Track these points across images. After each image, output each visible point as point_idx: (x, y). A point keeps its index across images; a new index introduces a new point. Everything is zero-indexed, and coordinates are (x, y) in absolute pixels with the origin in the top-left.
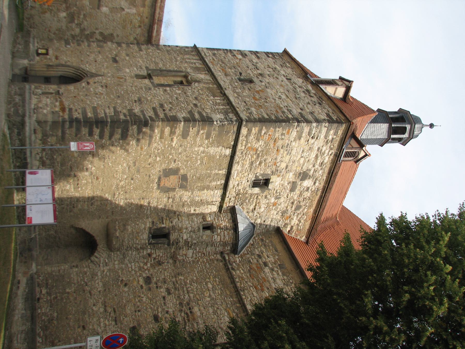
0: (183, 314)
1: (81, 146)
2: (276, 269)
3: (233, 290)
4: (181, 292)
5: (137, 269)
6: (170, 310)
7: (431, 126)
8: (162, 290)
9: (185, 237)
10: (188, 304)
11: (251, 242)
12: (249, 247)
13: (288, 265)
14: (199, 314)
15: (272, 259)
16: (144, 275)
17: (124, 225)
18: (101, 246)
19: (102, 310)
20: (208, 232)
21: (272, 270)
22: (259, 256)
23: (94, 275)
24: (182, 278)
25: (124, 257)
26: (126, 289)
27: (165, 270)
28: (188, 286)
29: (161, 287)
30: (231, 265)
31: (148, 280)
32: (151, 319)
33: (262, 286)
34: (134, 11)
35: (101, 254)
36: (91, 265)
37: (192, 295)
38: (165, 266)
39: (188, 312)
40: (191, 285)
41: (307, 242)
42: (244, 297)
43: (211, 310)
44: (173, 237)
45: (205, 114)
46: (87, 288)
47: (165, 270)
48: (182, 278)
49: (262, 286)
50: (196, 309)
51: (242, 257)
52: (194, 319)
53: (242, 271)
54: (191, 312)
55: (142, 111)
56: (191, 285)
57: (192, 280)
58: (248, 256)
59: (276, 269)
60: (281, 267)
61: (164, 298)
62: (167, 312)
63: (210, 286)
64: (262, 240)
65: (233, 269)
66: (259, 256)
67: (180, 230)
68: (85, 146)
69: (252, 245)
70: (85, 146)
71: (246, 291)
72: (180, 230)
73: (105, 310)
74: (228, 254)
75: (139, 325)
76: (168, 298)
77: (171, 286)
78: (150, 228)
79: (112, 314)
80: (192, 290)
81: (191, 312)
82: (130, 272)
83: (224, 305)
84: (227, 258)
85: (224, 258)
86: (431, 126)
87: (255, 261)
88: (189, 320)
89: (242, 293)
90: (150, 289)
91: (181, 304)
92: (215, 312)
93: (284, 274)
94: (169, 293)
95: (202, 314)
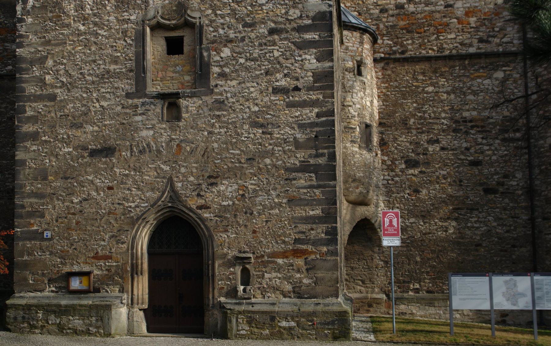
0: (472, 132)
3: (440, 63)
4: (436, 127)
5: (392, 174)
6: (465, 145)
8: (430, 149)
10: (456, 122)
14: (475, 113)
16: (403, 166)
24: (412, 120)
28: (426, 115)
31: (411, 164)
37: (443, 115)
39: (470, 124)
40: (425, 112)
42: (454, 52)
43: (471, 97)
48: (412, 120)
50: (466, 114)
52: (483, 120)
53: (410, 42)
54: (471, 121)
56: (425, 112)
58: (381, 26)
62: (467, 149)
63: (430, 89)
65: (403, 53)
68: (391, 224)
70: (391, 224)
71: (445, 46)
75: (481, 184)
77: (425, 137)
79: (463, 212)
80: (434, 112)
81: (471, 121)
82: (396, 182)
84: (383, 55)
87: (391, 19)
88: (482, 127)
89: (447, 53)
92: (475, 93)
94: (437, 141)
95: (474, 109)
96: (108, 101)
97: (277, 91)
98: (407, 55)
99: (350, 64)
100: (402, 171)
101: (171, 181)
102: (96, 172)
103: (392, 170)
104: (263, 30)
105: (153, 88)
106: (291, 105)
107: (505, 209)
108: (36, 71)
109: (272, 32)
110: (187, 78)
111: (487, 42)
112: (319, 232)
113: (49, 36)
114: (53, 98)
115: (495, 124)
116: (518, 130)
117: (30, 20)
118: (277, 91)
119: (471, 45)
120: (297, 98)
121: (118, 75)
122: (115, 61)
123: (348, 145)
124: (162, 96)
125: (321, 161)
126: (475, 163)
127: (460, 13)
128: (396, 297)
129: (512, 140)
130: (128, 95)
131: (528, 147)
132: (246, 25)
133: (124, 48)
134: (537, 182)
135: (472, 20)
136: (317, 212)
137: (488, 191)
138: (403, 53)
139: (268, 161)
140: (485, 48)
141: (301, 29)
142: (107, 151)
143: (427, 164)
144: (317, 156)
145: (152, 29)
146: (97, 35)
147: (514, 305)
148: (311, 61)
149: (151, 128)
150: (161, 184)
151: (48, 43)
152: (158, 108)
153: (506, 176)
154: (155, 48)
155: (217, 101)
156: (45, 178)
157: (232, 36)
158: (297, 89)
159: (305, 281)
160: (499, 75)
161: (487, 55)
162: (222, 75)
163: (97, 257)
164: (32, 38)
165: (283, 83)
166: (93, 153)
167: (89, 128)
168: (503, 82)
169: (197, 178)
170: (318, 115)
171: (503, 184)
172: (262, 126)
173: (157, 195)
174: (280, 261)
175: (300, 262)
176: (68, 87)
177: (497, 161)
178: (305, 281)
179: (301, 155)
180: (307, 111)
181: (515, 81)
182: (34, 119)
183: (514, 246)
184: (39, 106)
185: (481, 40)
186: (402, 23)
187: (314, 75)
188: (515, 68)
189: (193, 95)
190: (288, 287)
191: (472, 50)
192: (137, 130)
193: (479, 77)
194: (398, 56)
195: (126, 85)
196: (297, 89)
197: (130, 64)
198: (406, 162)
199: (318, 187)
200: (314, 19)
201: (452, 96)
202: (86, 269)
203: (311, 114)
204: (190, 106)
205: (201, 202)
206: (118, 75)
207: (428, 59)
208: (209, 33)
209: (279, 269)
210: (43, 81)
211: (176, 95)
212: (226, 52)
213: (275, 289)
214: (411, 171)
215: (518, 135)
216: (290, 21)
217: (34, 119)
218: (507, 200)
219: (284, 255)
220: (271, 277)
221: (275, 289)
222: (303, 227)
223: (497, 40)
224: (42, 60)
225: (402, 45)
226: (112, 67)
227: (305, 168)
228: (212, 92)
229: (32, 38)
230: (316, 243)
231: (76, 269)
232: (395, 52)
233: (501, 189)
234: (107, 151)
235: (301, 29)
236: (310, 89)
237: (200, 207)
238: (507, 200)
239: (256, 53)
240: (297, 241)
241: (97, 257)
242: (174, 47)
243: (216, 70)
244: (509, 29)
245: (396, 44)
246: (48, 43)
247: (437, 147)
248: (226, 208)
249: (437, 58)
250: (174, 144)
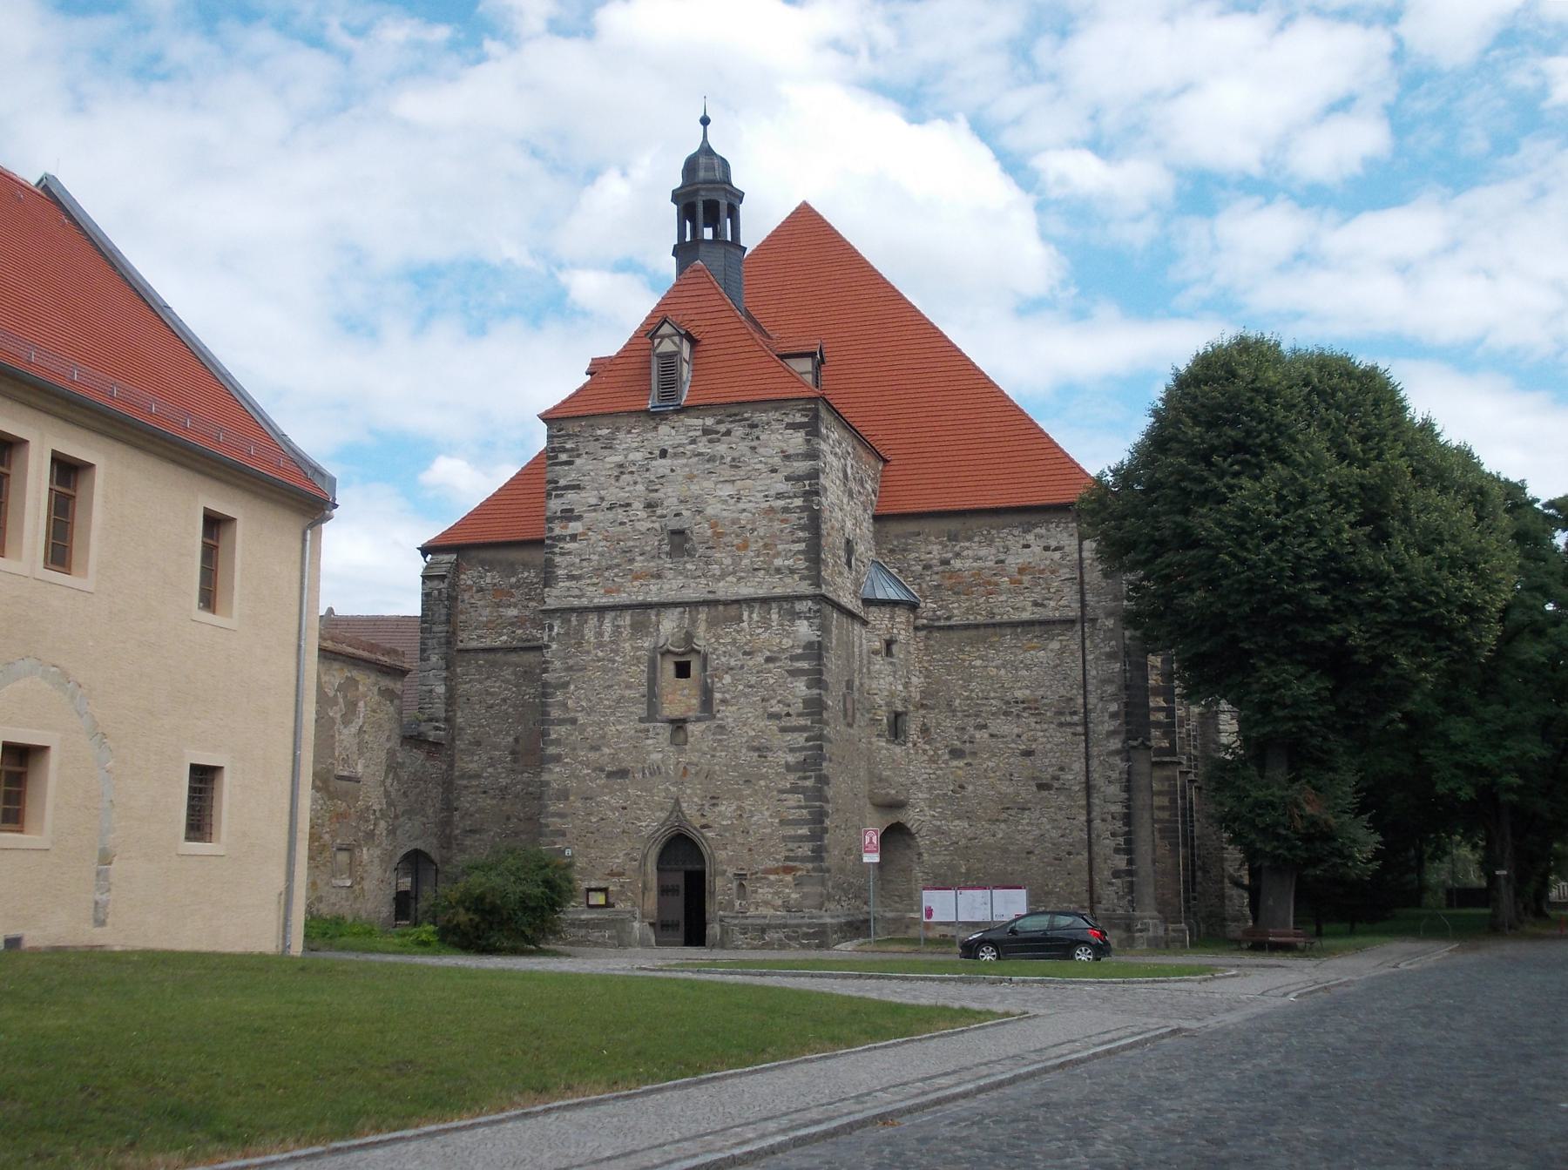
1: (871, 848)
2: (957, 549)
3: (990, 631)
6: (1016, 731)
7: (705, 121)
9: (900, 688)
10: (1008, 703)
11: (894, 571)
12: (906, 577)
13: (953, 525)
14: (1028, 692)
15: (936, 549)
16: (947, 757)
17: (880, 780)
18: (901, 817)
19: (1003, 826)
20: (895, 648)
21: (958, 555)
22: (927, 567)
23: (938, 831)
25: (870, 772)
26: (970, 788)
27: (939, 724)
29: (972, 737)
30: (939, 619)
31: (956, 753)
32: (1027, 761)
33: (989, 583)
34: (361, 704)
35: (911, 818)
36: (923, 833)
38: (931, 723)
41: (886, 461)
44: (900, 709)
45: (800, 651)
46: (963, 842)
47: (939, 724)
49: (989, 583)
50: (1019, 694)
51: (926, 597)
52: (1036, 701)
55: (792, 750)
57: (964, 687)
59: (957, 549)
60: (953, 537)
61: (992, 736)
62: (1019, 736)
63: (978, 663)
64: (892, 551)
65: (948, 618)
66: (926, 567)
67: (892, 694)
69: (900, 571)
72: (892, 694)
73: (1005, 821)
74: (916, 618)
76: (993, 730)
77: (972, 721)
78: (888, 741)
79: (1012, 812)
83: (1018, 651)
85: (924, 627)
86: (705, 121)
87: (935, 577)
90: (974, 754)
91: (1006, 714)
93: (970, 539)
94: (985, 727)
95: (1027, 687)
96: (623, 726)
97: (772, 716)
98: (952, 622)
99: (877, 645)
100: (946, 762)
101: (677, 802)
102: (612, 793)
103: (935, 762)
104: (760, 659)
105: (671, 709)
106: (783, 730)
107: (1060, 809)
108: (559, 696)
109: (768, 660)
110: (694, 701)
111: (1042, 605)
112: (806, 849)
113: (571, 662)
114: (574, 721)
115: (1050, 705)
116: (1075, 713)
117: (554, 646)
118: (772, 716)
119: (1024, 609)
120: (785, 722)
121: (634, 701)
122: (629, 686)
123: (874, 739)
124: (672, 721)
125: (809, 783)
126: (1028, 753)
127: (1013, 569)
128: (663, 928)
129: (1070, 724)
130: (641, 720)
131: (1086, 734)
132: (745, 653)
133: (639, 673)
134: (1096, 776)
135: (1026, 579)
136: (804, 831)
137: (1042, 786)
138: (948, 618)
139: (762, 783)
140: (1040, 614)
141: (793, 658)
142: (623, 773)
143: (974, 754)
144: (805, 778)
145: (663, 655)
146: (614, 662)
147: (678, 925)
148: (801, 687)
149: (657, 747)
150: (670, 804)
151: (570, 669)
152: (665, 731)
153: (1062, 769)
154: (669, 668)
155: (719, 726)
156: (567, 799)
157: (733, 663)
158: (788, 715)
159: (794, 896)
160: (1055, 645)
161: (1041, 623)
162: (724, 701)
163: (612, 874)
164: (558, 664)
165: (776, 709)
166: (610, 775)
167: (606, 750)
168: (1062, 650)
169: (702, 798)
170: (807, 740)
171: (1057, 778)
172: (758, 749)
173: (664, 815)
174: (772, 877)
175: (789, 878)
176: (589, 711)
177: (1051, 750)
178: (794, 896)
179: (791, 777)
180: (796, 735)
181: (1072, 654)
182: (557, 742)
183: (1069, 853)
184: (563, 729)
185: (1036, 604)
186: (947, 583)
187: (805, 702)
188: (1072, 638)
189: (698, 720)
190: (780, 902)
191: (1026, 616)
192: (648, 753)
193: (1033, 648)
194: (942, 623)
195: (641, 710)
196: (788, 715)
197: (643, 690)
198: (951, 752)
199: (805, 807)
200: (805, 648)
201: (1003, 672)
202: (603, 885)
203: (800, 739)
204: (694, 729)
205: (704, 821)
206: (634, 701)
207: (977, 626)
208: (714, 662)
209: (771, 885)
210: (565, 705)
211: (684, 721)
212: (727, 679)
213: (766, 903)
214: (955, 763)
215: (1076, 718)
216: (784, 651)
217: (557, 742)
218: (1062, 798)
219: (775, 871)
220: (764, 892)
221: (766, 903)
222: (791, 845)
223: (1052, 603)
224: (566, 685)
225: (950, 610)
226: (627, 693)
227: (794, 790)
228: (714, 717)
229: (558, 664)
230: (804, 859)
231: (594, 885)
232: (939, 619)
233: (1056, 785)
234: (623, 773)
235: (793, 658)
236: (799, 715)
237: (703, 827)
238: (1062, 798)
239: (753, 680)
240: (787, 858)
241: (612, 874)
242: (683, 670)
243: (718, 696)
244: (1066, 590)
245: (941, 607)
246: (570, 669)
247: (985, 734)
248: (726, 828)
249: (986, 626)
250: (681, 766)
